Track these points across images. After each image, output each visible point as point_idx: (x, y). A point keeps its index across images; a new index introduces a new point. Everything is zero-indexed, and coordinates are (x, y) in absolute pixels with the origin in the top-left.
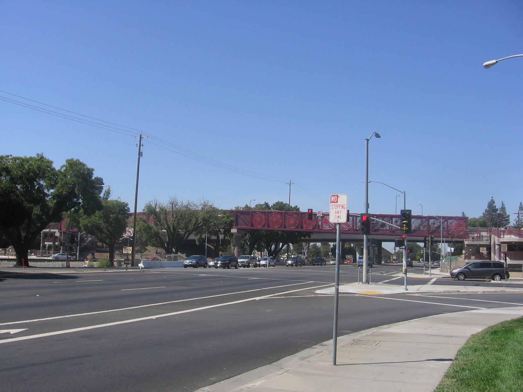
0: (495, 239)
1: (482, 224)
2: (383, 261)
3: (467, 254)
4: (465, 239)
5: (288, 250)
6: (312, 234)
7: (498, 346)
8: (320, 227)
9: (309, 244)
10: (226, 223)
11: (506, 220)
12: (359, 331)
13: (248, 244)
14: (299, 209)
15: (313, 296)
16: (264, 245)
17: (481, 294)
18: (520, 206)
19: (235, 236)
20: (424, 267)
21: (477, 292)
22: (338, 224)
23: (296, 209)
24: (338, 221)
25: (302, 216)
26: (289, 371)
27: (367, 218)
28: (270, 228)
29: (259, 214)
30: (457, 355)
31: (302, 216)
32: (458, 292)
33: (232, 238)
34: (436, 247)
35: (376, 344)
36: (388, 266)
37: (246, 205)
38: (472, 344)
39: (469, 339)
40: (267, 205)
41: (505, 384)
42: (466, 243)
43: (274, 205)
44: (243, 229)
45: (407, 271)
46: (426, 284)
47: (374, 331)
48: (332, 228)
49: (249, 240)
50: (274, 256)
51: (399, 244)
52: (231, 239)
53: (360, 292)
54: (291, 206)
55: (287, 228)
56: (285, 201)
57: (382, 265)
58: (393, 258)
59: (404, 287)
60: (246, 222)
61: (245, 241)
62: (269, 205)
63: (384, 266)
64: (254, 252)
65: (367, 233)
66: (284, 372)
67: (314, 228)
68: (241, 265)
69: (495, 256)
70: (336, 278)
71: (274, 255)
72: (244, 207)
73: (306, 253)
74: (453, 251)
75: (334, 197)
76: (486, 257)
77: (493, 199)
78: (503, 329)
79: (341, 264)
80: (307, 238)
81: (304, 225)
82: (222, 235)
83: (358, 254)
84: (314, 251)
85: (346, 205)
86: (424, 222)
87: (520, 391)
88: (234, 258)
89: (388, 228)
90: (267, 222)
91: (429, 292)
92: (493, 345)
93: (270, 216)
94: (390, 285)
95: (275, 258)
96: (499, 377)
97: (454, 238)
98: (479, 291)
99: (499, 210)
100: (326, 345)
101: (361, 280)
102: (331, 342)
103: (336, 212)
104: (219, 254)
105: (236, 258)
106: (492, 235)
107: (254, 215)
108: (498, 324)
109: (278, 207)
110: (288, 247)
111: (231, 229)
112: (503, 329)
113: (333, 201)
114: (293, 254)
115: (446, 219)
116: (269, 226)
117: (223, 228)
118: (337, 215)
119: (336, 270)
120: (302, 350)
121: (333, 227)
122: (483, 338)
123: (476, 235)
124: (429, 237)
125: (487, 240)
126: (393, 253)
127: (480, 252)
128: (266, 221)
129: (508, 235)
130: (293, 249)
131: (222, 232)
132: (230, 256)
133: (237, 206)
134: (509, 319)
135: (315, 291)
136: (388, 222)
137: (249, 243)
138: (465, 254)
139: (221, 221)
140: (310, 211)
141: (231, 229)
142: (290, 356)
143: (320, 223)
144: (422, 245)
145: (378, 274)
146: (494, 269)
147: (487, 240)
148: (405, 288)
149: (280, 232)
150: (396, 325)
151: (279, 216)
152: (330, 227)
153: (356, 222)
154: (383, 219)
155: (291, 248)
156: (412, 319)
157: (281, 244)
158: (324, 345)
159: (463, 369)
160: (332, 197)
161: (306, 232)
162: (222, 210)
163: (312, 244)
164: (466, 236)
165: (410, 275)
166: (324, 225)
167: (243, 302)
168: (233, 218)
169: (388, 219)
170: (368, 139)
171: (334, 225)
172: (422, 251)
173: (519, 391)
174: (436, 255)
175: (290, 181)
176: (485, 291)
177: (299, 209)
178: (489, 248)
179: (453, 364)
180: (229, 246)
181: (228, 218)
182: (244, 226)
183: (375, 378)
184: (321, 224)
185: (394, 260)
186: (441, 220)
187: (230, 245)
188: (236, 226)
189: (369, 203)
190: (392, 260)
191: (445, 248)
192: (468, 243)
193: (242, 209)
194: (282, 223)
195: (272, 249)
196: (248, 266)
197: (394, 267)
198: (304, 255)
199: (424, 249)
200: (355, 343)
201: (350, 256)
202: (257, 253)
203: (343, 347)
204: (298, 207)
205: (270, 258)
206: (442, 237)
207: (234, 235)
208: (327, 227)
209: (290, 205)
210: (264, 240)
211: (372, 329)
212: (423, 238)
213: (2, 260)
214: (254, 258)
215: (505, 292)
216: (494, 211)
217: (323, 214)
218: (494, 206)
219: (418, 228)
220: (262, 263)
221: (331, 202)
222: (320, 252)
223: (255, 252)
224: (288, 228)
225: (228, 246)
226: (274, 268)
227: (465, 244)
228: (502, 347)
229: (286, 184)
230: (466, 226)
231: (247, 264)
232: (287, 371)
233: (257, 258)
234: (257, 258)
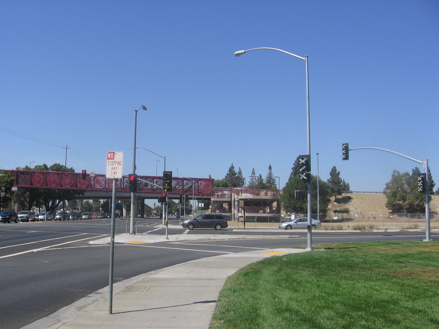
0: (235, 197)
1: (224, 185)
2: (145, 215)
3: (213, 209)
4: (211, 197)
5: (64, 206)
6: (85, 192)
7: (252, 286)
8: (92, 186)
9: (82, 201)
10: (7, 182)
11: (242, 182)
12: (130, 278)
13: (27, 200)
14: (74, 170)
15: (87, 246)
16: (43, 202)
17: (227, 241)
18: (253, 171)
19: (16, 194)
20: (180, 219)
21: (224, 239)
22: (114, 179)
23: (72, 170)
24: (114, 177)
25: (76, 177)
26: (66, 324)
27: (135, 178)
28: (48, 187)
29: (37, 174)
30: (220, 297)
31: (76, 177)
32: (209, 240)
33: (13, 196)
34: (188, 203)
35: (146, 290)
36: (149, 219)
37: (26, 166)
38: (230, 285)
39: (226, 281)
40: (45, 166)
41: (267, 322)
42: (212, 199)
43: (52, 166)
44: (24, 188)
45: (168, 223)
46: (182, 233)
47: (144, 278)
48: (102, 187)
49: (28, 198)
50: (51, 211)
51: (162, 200)
52: (11, 197)
53: (128, 242)
54: (67, 168)
55: (63, 187)
56: (62, 163)
57: (145, 218)
58: (154, 212)
59: (165, 236)
60: (26, 181)
61: (25, 198)
62: (47, 166)
63: (146, 219)
64: (33, 208)
65: (134, 191)
66: (61, 325)
67: (87, 187)
68: (20, 220)
69: (235, 210)
70: (112, 231)
71: (52, 210)
72: (24, 168)
73: (79, 209)
74: (203, 207)
75: (111, 154)
76: (228, 211)
77: (233, 165)
78: (252, 270)
79: (116, 218)
80: (81, 195)
81: (79, 185)
82: (3, 192)
83: (125, 210)
84: (87, 207)
85: (122, 161)
86: (179, 182)
87: (280, 328)
88: (14, 213)
89: (150, 187)
90: (45, 181)
91: (186, 240)
92: (248, 285)
93: (48, 176)
94: (153, 235)
95: (52, 213)
96: (260, 315)
97: (204, 196)
98: (225, 238)
99: (237, 174)
100: (101, 293)
101: (128, 231)
102: (107, 289)
103: (112, 168)
104: (1, 210)
105: (16, 213)
106: (233, 194)
107: (34, 175)
108: (247, 266)
109: (55, 168)
110: (64, 203)
111: (12, 188)
112: (252, 270)
113: (110, 158)
114: (68, 210)
115: (197, 180)
116: (47, 185)
117: (4, 187)
118: (114, 171)
119: (112, 223)
120: (79, 300)
121: (103, 186)
122: (238, 279)
123: (220, 193)
124: (184, 195)
125: (229, 198)
126: (153, 208)
127: (223, 207)
128: (44, 181)
129: (244, 193)
130: (68, 205)
131: (3, 190)
132: (10, 212)
133: (17, 167)
134: (254, 261)
135: (89, 242)
136: (150, 182)
137: (28, 200)
138: (211, 209)
139: (2, 180)
140: (84, 172)
141: (12, 188)
142: (67, 306)
143: (92, 183)
144: (177, 201)
145: (143, 226)
146: (216, 220)
147: (229, 198)
148: (166, 237)
149: (57, 190)
150: (163, 271)
151: (56, 176)
152: (101, 186)
153: (123, 182)
154: (146, 180)
155: (67, 204)
156: (174, 265)
157: (58, 201)
158: (99, 293)
159: (228, 311)
160: (109, 154)
161: (80, 190)
162: (3, 170)
163: (85, 200)
164: (212, 194)
165: (170, 226)
166: (96, 185)
167: (20, 254)
168: (14, 178)
169: (151, 180)
170: (137, 111)
171: (104, 185)
172: (178, 206)
173: (280, 328)
174: (188, 210)
175: (67, 146)
176: (230, 238)
177: (74, 171)
178: (230, 204)
179: (217, 305)
180: (10, 203)
181: (9, 177)
182: (24, 185)
183: (150, 325)
184: (93, 184)
185: (154, 214)
186: (193, 181)
187: (10, 202)
188: (16, 185)
189: (136, 165)
190: (152, 214)
191: (194, 204)
192: (214, 199)
193: (22, 170)
194: (59, 182)
195: (49, 205)
196: (27, 221)
197: (154, 219)
198: (78, 210)
199: (180, 204)
200: (128, 290)
201: (117, 211)
202: (35, 208)
203: (117, 294)
204: (73, 169)
205: (47, 213)
206: (194, 195)
207: (14, 192)
208: (98, 186)
209: (66, 167)
210: (42, 197)
211: (142, 275)
212: (179, 196)
213: (438, 228)
214: (34, 213)
215: (245, 239)
216: (234, 175)
217: (95, 175)
218: (233, 170)
219: (174, 187)
220: (40, 217)
221: (108, 159)
222: (92, 208)
223: (34, 208)
224: (64, 187)
225: (9, 202)
226: (51, 222)
227: (212, 200)
228: (255, 287)
229: (63, 148)
230: (212, 186)
231: (27, 219)
232: (64, 324)
233: (36, 214)
234: (36, 214)
